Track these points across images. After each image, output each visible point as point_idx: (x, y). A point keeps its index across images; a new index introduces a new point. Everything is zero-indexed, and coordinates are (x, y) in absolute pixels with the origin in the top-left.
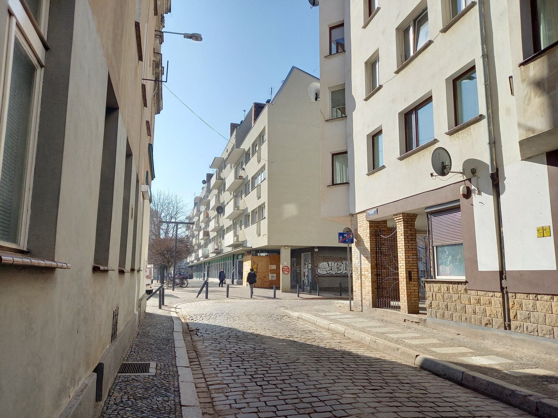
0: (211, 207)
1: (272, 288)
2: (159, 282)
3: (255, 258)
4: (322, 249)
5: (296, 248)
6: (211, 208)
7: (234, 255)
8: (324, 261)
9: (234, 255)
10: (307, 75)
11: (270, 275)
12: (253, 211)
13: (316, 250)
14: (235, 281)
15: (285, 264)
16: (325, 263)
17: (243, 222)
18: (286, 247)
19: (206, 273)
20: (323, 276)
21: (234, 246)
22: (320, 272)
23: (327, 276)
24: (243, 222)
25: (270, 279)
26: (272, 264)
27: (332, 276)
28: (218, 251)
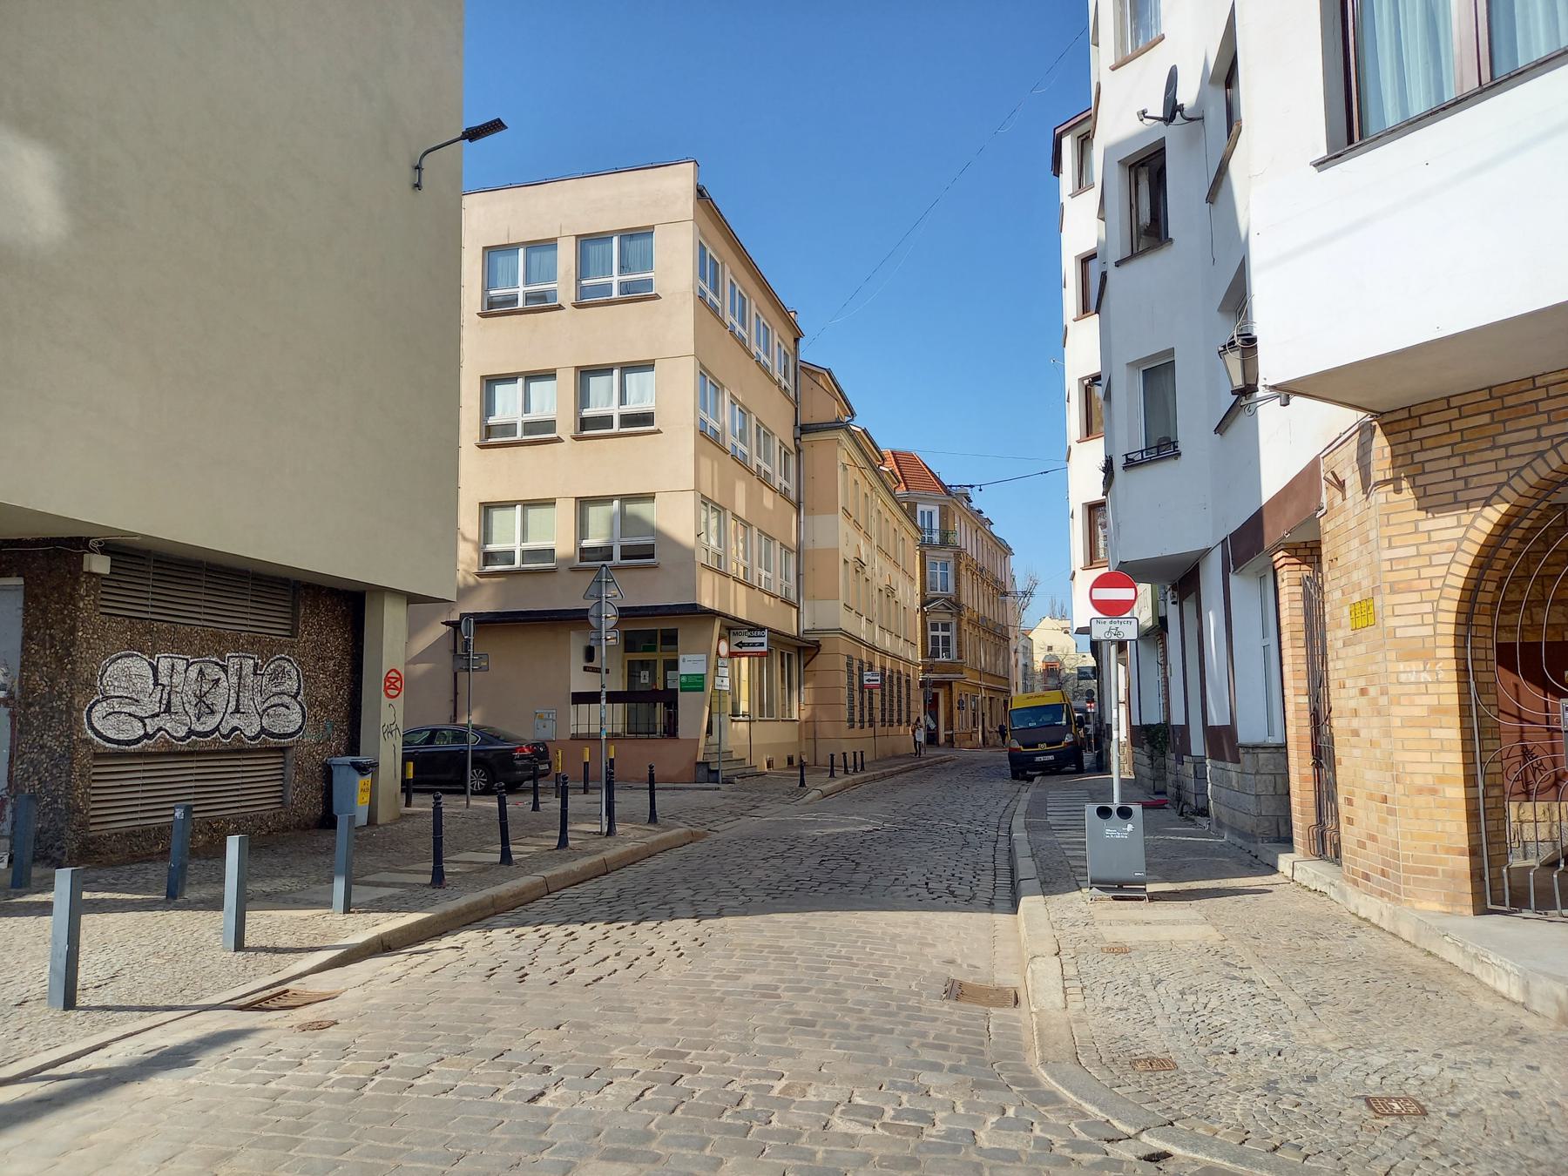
16: (138, 666)
20: (123, 753)
22: (110, 723)
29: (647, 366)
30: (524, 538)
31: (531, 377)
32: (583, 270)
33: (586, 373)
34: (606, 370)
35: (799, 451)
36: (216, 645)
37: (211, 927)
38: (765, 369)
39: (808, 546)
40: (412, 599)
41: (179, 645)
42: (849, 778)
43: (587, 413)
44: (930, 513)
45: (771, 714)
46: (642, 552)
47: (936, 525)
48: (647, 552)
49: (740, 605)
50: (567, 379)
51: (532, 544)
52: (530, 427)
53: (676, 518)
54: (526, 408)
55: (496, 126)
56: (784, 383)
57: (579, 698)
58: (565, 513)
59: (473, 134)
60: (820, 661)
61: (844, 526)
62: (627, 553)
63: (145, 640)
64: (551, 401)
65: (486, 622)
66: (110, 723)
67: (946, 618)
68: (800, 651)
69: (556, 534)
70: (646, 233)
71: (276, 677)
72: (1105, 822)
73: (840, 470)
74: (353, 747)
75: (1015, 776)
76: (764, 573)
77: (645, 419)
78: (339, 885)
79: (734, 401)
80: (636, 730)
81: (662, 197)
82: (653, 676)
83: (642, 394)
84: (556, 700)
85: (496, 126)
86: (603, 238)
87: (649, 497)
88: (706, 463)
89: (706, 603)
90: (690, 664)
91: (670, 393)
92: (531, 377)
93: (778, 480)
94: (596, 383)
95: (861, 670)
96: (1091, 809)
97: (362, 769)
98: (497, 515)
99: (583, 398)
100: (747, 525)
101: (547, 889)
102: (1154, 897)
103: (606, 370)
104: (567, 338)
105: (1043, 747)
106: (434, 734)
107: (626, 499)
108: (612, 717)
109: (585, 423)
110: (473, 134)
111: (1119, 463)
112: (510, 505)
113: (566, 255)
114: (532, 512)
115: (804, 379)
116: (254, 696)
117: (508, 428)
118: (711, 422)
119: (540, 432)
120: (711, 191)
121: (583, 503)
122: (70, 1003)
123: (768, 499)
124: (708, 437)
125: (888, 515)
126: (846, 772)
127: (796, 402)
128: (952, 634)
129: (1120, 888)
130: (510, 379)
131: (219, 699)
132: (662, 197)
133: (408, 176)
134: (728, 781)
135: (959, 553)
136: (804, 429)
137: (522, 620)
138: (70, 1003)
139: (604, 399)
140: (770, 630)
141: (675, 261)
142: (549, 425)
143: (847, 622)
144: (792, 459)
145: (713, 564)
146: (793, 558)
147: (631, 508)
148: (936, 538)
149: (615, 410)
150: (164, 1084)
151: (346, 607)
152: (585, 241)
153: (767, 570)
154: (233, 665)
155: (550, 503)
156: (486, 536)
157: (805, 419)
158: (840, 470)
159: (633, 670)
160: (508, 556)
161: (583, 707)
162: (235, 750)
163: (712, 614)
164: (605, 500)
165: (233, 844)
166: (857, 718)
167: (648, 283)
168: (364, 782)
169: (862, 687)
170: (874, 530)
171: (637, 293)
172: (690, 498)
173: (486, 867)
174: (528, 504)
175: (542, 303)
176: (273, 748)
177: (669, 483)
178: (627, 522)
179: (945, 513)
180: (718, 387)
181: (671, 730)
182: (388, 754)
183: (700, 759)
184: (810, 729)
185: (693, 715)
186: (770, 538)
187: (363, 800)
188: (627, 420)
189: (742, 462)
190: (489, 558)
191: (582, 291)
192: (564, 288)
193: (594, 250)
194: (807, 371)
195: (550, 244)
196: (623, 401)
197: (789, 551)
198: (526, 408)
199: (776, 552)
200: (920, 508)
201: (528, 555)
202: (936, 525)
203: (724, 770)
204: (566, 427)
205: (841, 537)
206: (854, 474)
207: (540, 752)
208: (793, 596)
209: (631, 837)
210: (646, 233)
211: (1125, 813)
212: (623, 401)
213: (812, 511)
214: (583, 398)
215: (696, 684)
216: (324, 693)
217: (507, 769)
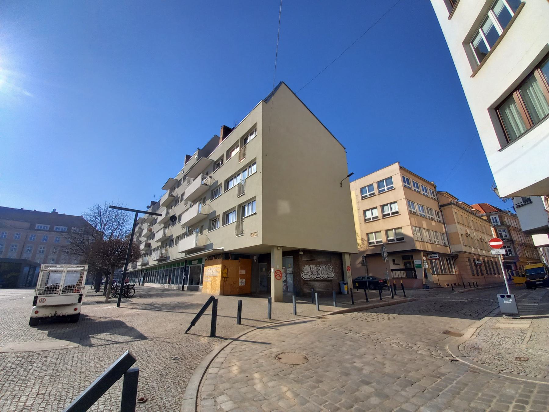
0: (143, 234)
1: (291, 302)
2: (93, 287)
3: (226, 261)
4: (307, 252)
5: (293, 249)
6: (143, 235)
7: (186, 261)
8: (307, 265)
9: (186, 261)
10: (297, 99)
11: (240, 280)
12: (177, 237)
13: (301, 253)
14: (186, 286)
15: (278, 267)
16: (308, 267)
17: (168, 244)
18: (279, 248)
19: (142, 279)
20: (307, 281)
21: (159, 260)
22: (305, 276)
23: (317, 281)
24: (168, 244)
25: (240, 285)
26: (242, 269)
27: (313, 281)
28: (162, 259)
29: (395, 202)
30: (376, 239)
31: (372, 209)
32: (379, 187)
33: (382, 206)
34: (387, 205)
35: (441, 211)
36: (318, 263)
37: (315, 307)
38: (427, 196)
39: (449, 232)
40: (350, 254)
41: (314, 264)
42: (470, 289)
43: (384, 213)
44: (495, 218)
45: (445, 272)
46: (401, 239)
47: (498, 220)
48: (402, 239)
49: (429, 248)
50: (379, 208)
51: (378, 240)
52: (373, 218)
53: (408, 231)
54: (372, 215)
55: (352, 173)
56: (433, 197)
57: (393, 270)
58: (383, 234)
59: (349, 176)
60: (459, 259)
61: (458, 226)
62: (398, 240)
63: (309, 264)
64: (376, 213)
65: (368, 256)
66: (305, 276)
67: (509, 245)
68: (453, 258)
69: (382, 238)
70: (390, 178)
71: (329, 268)
72: (503, 299)
73: (454, 214)
74: (343, 280)
75: (527, 288)
76: (436, 240)
77: (397, 212)
78: (334, 303)
79: (418, 205)
80: (408, 276)
81: (393, 171)
82: (410, 265)
83: (395, 208)
84: (390, 271)
85: (352, 173)
86: (382, 181)
87: (400, 228)
88: (413, 219)
89: (419, 248)
90: (417, 262)
91: (401, 206)
92: (372, 209)
93: (436, 219)
94: (385, 208)
95: (474, 261)
96: (499, 296)
97: (345, 284)
98: (370, 235)
99: (383, 211)
100: (428, 230)
101: (375, 307)
102: (522, 318)
103: (387, 205)
104: (379, 200)
105: (538, 279)
106: (363, 278)
107: (395, 229)
108: (402, 274)
109: (384, 216)
110: (349, 176)
111: (515, 206)
112: (372, 233)
113: (375, 186)
114: (377, 234)
115: (439, 195)
116: (326, 272)
117: (370, 219)
118: (413, 210)
119: (376, 219)
120: (403, 166)
121: (387, 231)
122: (296, 314)
123: (433, 223)
124: (412, 213)
125: (476, 221)
126: (474, 287)
127: (438, 201)
128: (512, 248)
129: (514, 316)
130: (368, 210)
131: (320, 272)
132: (393, 171)
133: (339, 185)
134: (432, 288)
135: (508, 227)
136: (441, 206)
137: (374, 255)
138: (296, 314)
139: (387, 210)
140: (438, 253)
141: (398, 181)
142: (377, 217)
143: (465, 249)
144: (440, 214)
145: (420, 240)
146: (445, 236)
147: (397, 231)
148: (499, 224)
149: (390, 212)
150: (302, 325)
151: (339, 256)
152: (378, 183)
153: (437, 239)
154: (322, 267)
155: (380, 232)
156: (368, 239)
157: (441, 203)
158: (454, 214)
159: (405, 264)
160: (373, 243)
161: (394, 272)
162: (324, 280)
163: (420, 251)
164: (391, 230)
165: (316, 294)
166: (475, 273)
167: (393, 187)
168: (345, 286)
169: (476, 265)
170: (471, 225)
171: (392, 189)
172: (410, 227)
173: (364, 302)
174: (375, 232)
175: (373, 195)
176: (330, 280)
177: (405, 225)
178: (396, 234)
179: (500, 217)
180: (413, 203)
181: (416, 277)
182: (350, 281)
183: (424, 283)
184: (460, 276)
185: (421, 274)
186: (436, 232)
187: (346, 289)
188: (393, 213)
189: (424, 217)
190: (370, 243)
191: (380, 191)
192: (376, 191)
193: (381, 184)
194: (441, 193)
195: (372, 185)
196: (391, 210)
197: (443, 234)
198: (372, 215)
199: (439, 235)
200: (491, 217)
201: (377, 242)
202: (498, 220)
203: (430, 286)
204: (380, 217)
205: (460, 229)
206: (459, 214)
207: (385, 282)
208: (447, 244)
209: (397, 299)
210: (390, 178)
211: (509, 297)
212: (391, 210)
213: (448, 224)
214: (383, 211)
215: (420, 266)
216: (337, 271)
217: (379, 285)
